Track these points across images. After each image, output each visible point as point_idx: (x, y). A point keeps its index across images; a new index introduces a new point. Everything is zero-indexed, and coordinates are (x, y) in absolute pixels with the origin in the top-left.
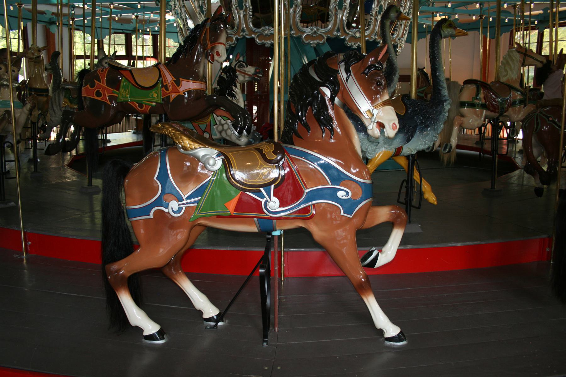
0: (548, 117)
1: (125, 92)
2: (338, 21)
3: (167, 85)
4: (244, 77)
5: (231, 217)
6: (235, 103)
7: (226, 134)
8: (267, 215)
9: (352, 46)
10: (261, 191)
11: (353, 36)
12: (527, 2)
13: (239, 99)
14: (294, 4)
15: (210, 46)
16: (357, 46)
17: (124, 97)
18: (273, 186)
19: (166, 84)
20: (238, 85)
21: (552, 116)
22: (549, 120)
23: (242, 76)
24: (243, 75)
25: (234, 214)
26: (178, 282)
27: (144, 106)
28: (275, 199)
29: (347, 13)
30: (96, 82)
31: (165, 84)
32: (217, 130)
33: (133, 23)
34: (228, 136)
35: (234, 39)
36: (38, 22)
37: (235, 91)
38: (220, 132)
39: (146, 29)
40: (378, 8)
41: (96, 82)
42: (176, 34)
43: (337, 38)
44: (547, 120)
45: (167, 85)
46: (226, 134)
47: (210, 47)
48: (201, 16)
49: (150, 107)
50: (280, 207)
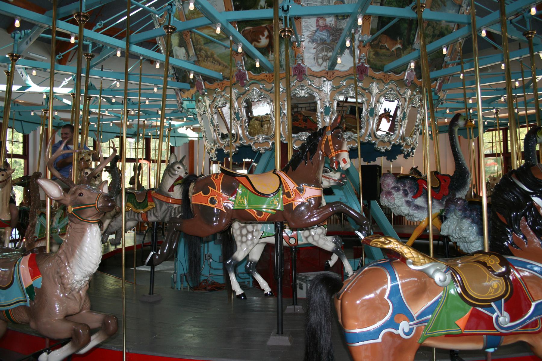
1: (242, 199)
2: (370, 128)
3: (289, 192)
4: (329, 182)
5: (461, 335)
7: (313, 239)
8: (498, 331)
9: (381, 150)
10: (491, 306)
11: (382, 141)
14: (330, 111)
15: (334, 154)
16: (385, 150)
17: (241, 205)
18: (503, 300)
19: (287, 191)
23: (327, 181)
24: (328, 180)
25: (464, 332)
27: (264, 213)
28: (505, 314)
29: (377, 120)
30: (211, 188)
31: (286, 191)
32: (303, 235)
33: (133, 127)
34: (315, 241)
35: (271, 143)
38: (307, 238)
39: (148, 133)
40: (402, 115)
41: (211, 188)
42: (174, 138)
43: (369, 143)
45: (289, 192)
46: (313, 239)
47: (335, 154)
48: (236, 122)
49: (270, 214)
50: (512, 320)
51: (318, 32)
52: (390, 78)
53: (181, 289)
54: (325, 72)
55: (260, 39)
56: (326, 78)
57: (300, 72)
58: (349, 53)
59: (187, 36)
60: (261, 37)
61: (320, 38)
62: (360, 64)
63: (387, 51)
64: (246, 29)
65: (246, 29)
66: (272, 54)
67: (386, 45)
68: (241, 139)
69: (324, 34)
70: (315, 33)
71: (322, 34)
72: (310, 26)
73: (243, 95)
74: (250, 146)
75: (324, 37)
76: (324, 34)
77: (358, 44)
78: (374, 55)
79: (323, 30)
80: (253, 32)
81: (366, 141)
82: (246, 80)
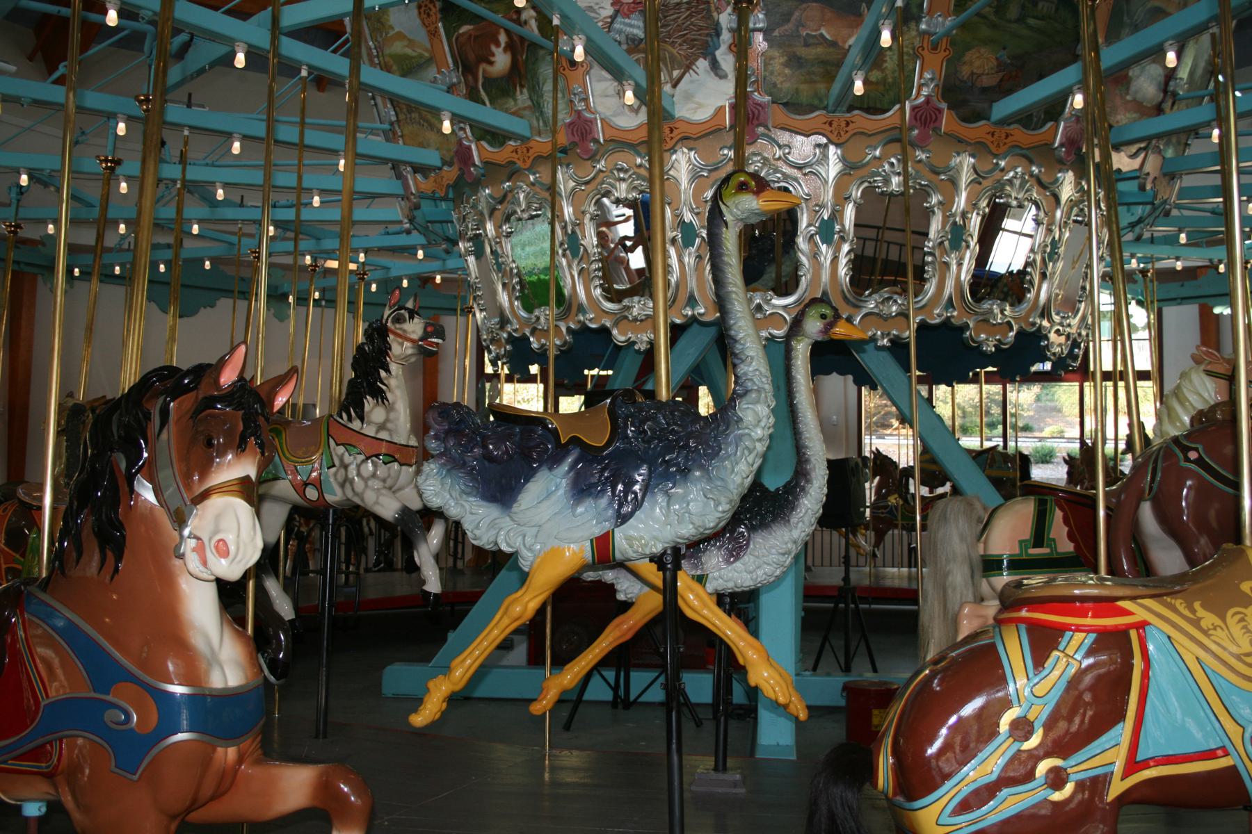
0: (1185, 450)
6: (697, 280)
12: (703, 391)
13: (394, 403)
20: (393, 367)
21: (1200, 448)
22: (1187, 460)
26: (846, 409)
32: (336, 479)
36: (709, 58)
37: (386, 382)
44: (1181, 456)
51: (619, 19)
52: (675, 132)
53: (1119, 318)
54: (825, 120)
55: (493, 55)
56: (824, 135)
57: (582, 133)
58: (708, 69)
59: (429, 15)
60: (493, 48)
61: (627, 36)
62: (922, 99)
63: (831, 50)
64: (461, 31)
65: (461, 31)
66: (521, 93)
67: (823, 31)
68: (581, 309)
69: (636, 23)
70: (612, 23)
71: (631, 26)
72: (596, 7)
73: (501, 202)
74: (604, 332)
75: (636, 31)
76: (636, 23)
77: (731, 41)
78: (786, 65)
79: (632, 12)
80: (476, 37)
81: (938, 321)
82: (597, 141)
